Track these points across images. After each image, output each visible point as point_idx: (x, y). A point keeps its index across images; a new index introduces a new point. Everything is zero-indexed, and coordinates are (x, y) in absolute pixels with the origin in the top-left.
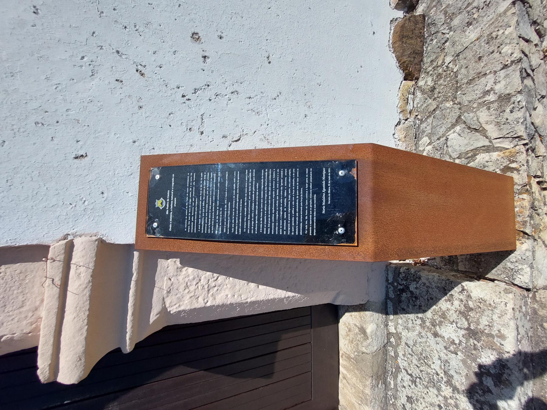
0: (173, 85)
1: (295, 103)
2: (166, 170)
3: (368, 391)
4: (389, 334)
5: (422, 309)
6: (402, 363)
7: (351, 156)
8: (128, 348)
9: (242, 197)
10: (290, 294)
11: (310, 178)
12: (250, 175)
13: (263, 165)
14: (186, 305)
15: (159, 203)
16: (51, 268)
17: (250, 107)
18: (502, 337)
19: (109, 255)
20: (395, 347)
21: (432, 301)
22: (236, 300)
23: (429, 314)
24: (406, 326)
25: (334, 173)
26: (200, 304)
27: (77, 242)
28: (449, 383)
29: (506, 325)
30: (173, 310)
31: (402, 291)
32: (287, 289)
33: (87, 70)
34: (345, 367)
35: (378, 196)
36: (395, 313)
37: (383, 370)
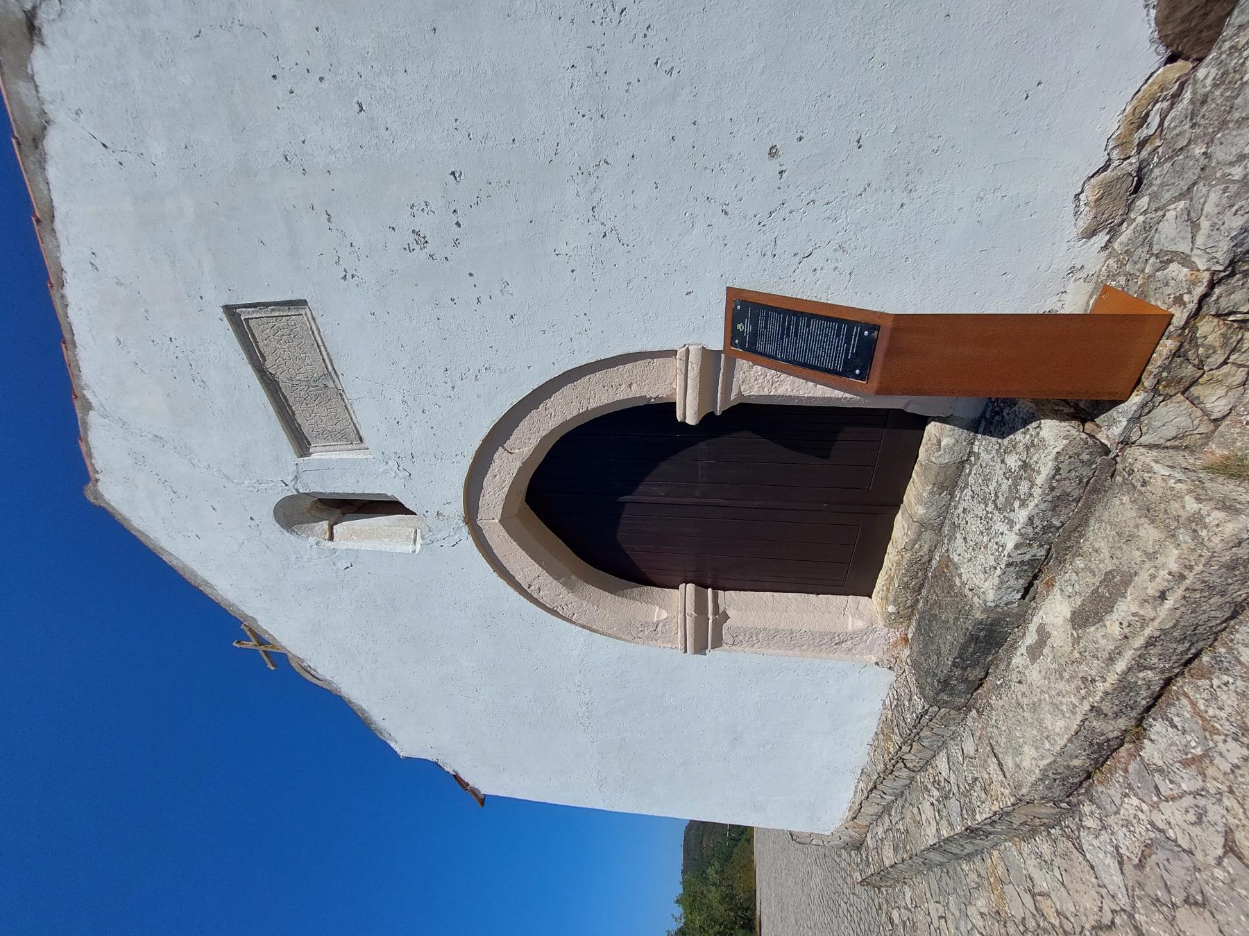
0: (751, 214)
1: (889, 192)
2: (744, 303)
3: (925, 495)
4: (971, 453)
5: (1003, 436)
6: (971, 480)
7: (878, 322)
8: (718, 413)
9: (796, 335)
10: (848, 395)
11: (844, 332)
12: (803, 321)
13: (811, 316)
14: (755, 392)
15: (739, 326)
16: (678, 363)
17: (827, 214)
18: (1039, 473)
19: (709, 357)
20: (972, 465)
21: (1013, 430)
22: (795, 393)
23: (1006, 441)
24: (985, 445)
25: (862, 332)
26: (766, 392)
27: (691, 348)
28: (994, 502)
29: (1045, 464)
30: (746, 394)
31: (997, 413)
32: (846, 391)
33: (689, 223)
34: (918, 475)
35: (889, 353)
36: (984, 434)
37: (950, 481)
